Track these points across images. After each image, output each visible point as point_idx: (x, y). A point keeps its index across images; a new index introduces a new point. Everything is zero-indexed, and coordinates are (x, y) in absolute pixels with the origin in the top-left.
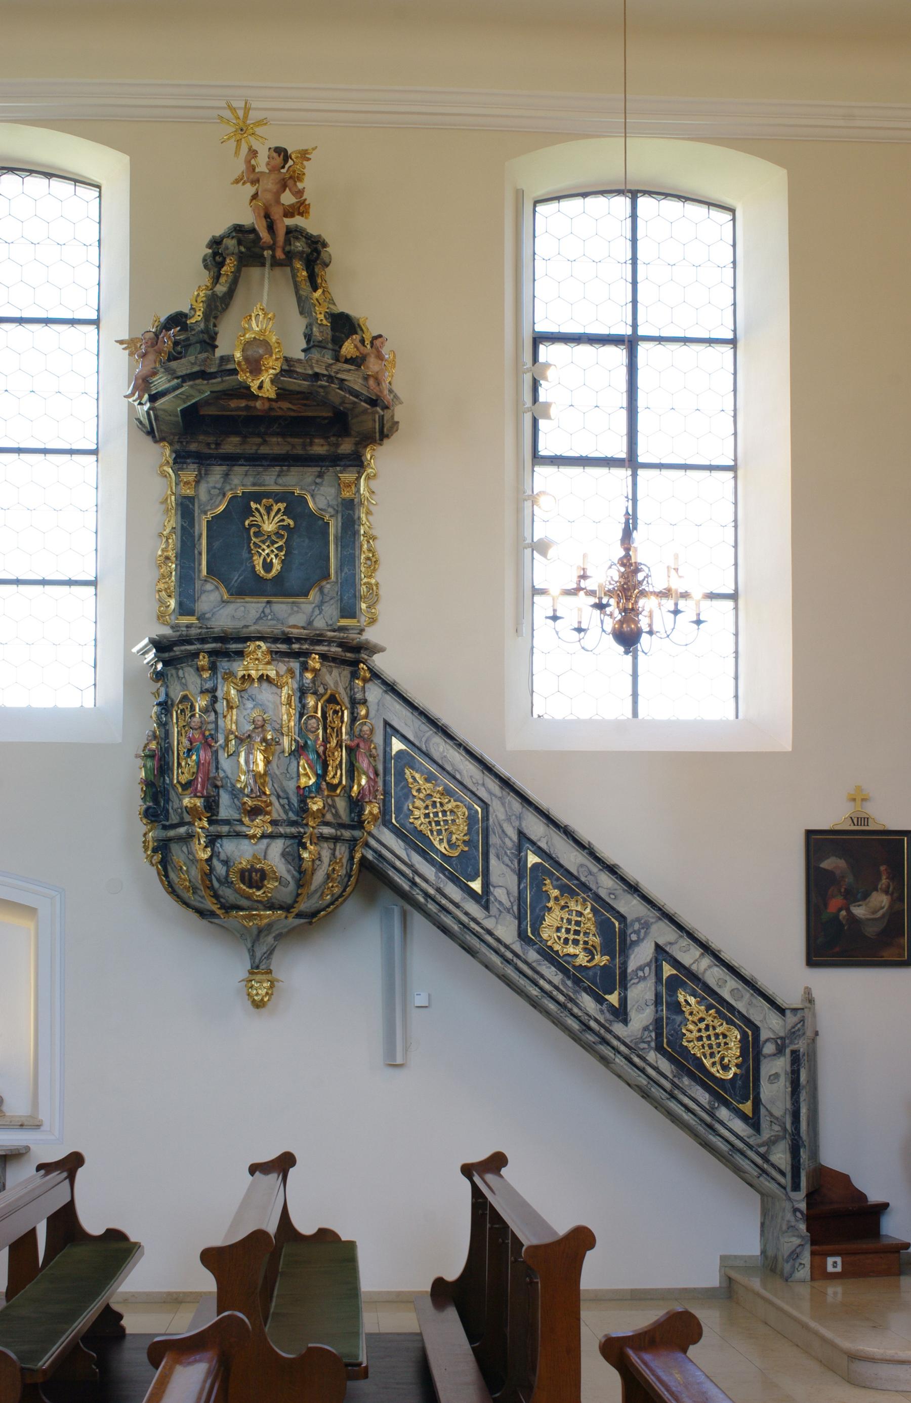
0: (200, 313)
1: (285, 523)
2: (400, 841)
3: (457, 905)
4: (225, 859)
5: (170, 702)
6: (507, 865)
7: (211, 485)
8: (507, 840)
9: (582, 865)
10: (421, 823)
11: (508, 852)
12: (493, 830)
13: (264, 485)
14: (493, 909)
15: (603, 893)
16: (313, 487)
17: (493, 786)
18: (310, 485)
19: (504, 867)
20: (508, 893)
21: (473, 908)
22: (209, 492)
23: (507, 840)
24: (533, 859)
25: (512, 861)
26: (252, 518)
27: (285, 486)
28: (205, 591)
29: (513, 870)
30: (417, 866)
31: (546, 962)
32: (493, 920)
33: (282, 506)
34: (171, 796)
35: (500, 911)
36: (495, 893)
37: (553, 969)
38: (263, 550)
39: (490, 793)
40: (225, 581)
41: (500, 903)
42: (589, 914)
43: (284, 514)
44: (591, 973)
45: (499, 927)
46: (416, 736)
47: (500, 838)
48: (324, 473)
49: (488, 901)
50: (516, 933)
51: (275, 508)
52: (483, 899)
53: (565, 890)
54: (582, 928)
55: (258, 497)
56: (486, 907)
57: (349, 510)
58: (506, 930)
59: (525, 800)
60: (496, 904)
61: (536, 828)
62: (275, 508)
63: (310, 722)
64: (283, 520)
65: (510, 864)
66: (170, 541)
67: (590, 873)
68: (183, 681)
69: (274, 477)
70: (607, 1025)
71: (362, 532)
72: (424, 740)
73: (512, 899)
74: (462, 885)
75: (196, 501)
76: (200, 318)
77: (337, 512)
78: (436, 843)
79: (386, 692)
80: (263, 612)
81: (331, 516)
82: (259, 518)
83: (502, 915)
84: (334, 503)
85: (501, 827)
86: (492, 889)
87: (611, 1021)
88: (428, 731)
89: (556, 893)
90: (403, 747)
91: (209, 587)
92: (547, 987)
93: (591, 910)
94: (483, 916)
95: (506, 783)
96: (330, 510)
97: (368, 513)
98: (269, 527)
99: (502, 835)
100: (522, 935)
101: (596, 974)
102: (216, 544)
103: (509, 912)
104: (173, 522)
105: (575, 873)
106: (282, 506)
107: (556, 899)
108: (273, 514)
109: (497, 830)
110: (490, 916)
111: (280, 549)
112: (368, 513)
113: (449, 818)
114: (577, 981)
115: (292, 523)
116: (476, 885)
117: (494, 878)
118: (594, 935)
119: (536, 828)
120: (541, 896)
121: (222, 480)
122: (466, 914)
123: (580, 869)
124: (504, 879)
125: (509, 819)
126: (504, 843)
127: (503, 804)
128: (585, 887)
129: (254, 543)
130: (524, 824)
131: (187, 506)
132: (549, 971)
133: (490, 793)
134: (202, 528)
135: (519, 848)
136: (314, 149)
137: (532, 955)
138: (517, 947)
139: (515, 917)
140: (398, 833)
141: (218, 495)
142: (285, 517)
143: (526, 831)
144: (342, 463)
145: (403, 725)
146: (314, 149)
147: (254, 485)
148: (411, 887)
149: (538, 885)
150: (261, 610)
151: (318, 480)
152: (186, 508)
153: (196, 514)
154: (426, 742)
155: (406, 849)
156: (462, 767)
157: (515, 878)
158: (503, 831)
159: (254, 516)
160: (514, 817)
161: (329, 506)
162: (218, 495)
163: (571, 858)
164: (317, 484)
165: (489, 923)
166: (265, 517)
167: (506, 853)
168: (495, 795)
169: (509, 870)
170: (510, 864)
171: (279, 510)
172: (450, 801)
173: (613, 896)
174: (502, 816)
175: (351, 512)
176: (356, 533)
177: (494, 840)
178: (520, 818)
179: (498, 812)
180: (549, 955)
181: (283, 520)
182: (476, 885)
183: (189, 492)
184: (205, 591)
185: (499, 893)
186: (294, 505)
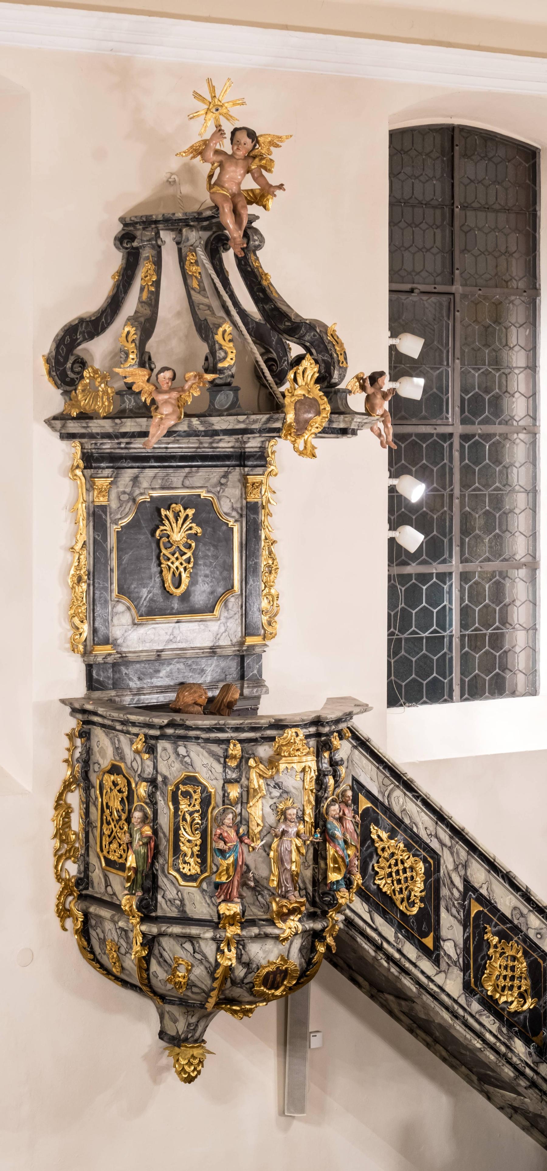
0: (232, 356)
1: (193, 532)
2: (364, 904)
3: (415, 965)
4: (247, 961)
5: (160, 779)
6: (455, 917)
7: (121, 489)
8: (455, 891)
9: (515, 908)
10: (385, 885)
11: (456, 902)
12: (443, 881)
13: (173, 488)
14: (443, 966)
15: (531, 934)
16: (218, 489)
17: (444, 835)
18: (215, 486)
19: (451, 918)
20: (455, 946)
21: (426, 965)
22: (119, 498)
23: (455, 891)
24: (476, 908)
25: (458, 912)
26: (162, 528)
27: (192, 488)
28: (117, 613)
29: (458, 921)
30: (380, 929)
31: (486, 1012)
32: (442, 975)
33: (191, 512)
34: (160, 883)
35: (449, 965)
36: (445, 948)
37: (492, 1018)
38: (173, 563)
39: (442, 844)
40: (134, 599)
41: (449, 957)
42: (521, 957)
43: (193, 521)
44: (522, 1017)
45: (448, 981)
46: (380, 792)
47: (449, 889)
48: (230, 472)
49: (438, 956)
50: (461, 986)
51: (183, 515)
52: (433, 954)
53: (503, 936)
54: (517, 973)
55: (168, 502)
56: (437, 962)
57: (252, 514)
58: (453, 984)
59: (472, 848)
60: (445, 958)
61: (479, 874)
62: (183, 515)
63: (332, 808)
64: (191, 528)
65: (457, 915)
66: (82, 557)
67: (522, 915)
68: (187, 759)
69: (181, 479)
70: (536, 1068)
71: (263, 537)
72: (386, 794)
73: (458, 951)
74: (416, 942)
75: (108, 508)
76: (232, 362)
77: (241, 516)
78: (398, 903)
79: (355, 747)
80: (172, 634)
81: (236, 521)
82: (168, 527)
83: (451, 968)
84: (238, 505)
85: (450, 878)
86: (442, 943)
87: (537, 1063)
88: (391, 784)
89: (496, 939)
90: (369, 805)
91: (120, 608)
92: (492, 1039)
93: (523, 953)
94: (435, 972)
95: (457, 833)
96: (234, 514)
97: (269, 514)
98: (178, 536)
99: (451, 886)
100: (467, 987)
101: (525, 1017)
102: (126, 558)
103: (456, 966)
104: (84, 533)
105: (510, 917)
106: (191, 512)
107: (496, 947)
108: (180, 521)
109: (447, 881)
110: (440, 972)
111: (188, 561)
112: (269, 514)
113: (409, 874)
114: (511, 1026)
115: (199, 530)
116: (429, 941)
117: (444, 932)
118: (525, 978)
119: (479, 874)
120: (482, 945)
121: (131, 483)
122: (423, 972)
123: (515, 912)
124: (451, 930)
125: (456, 869)
126: (452, 894)
127: (452, 854)
128: (516, 929)
129: (164, 554)
130: (468, 874)
131: (100, 516)
132: (489, 1022)
133: (442, 844)
134: (112, 540)
135: (464, 896)
136: (288, 137)
137: (475, 1007)
138: (462, 1001)
139: (461, 970)
140: (363, 894)
141: (128, 501)
142: (194, 525)
143: (470, 879)
144: (250, 463)
145: (369, 780)
146: (288, 137)
147: (163, 488)
148: (375, 951)
149: (480, 932)
150: (170, 632)
151: (223, 481)
152: (97, 517)
153: (108, 525)
154: (388, 796)
155: (370, 912)
156: (417, 820)
157: (461, 928)
158: (452, 882)
159: (164, 525)
160: (460, 866)
161: (233, 509)
162: (128, 501)
163: (506, 901)
164: (222, 484)
165: (439, 979)
166: (174, 525)
167: (453, 903)
168: (446, 846)
169: (456, 921)
170: (457, 915)
171: (187, 516)
172: (409, 857)
173: (539, 936)
174: (451, 867)
175: (255, 516)
176: (258, 538)
177: (444, 892)
178: (465, 866)
179: (447, 862)
180: (490, 1005)
181: (191, 528)
182: (429, 941)
183: (102, 500)
184: (117, 613)
185: (448, 947)
186: (204, 512)
